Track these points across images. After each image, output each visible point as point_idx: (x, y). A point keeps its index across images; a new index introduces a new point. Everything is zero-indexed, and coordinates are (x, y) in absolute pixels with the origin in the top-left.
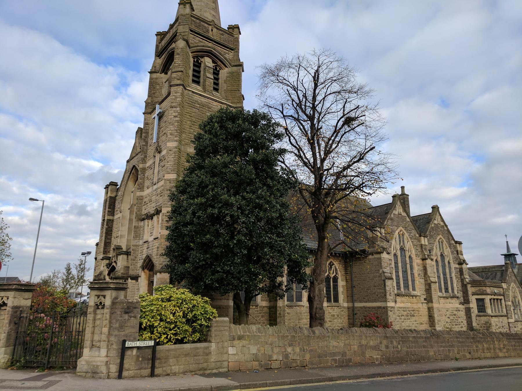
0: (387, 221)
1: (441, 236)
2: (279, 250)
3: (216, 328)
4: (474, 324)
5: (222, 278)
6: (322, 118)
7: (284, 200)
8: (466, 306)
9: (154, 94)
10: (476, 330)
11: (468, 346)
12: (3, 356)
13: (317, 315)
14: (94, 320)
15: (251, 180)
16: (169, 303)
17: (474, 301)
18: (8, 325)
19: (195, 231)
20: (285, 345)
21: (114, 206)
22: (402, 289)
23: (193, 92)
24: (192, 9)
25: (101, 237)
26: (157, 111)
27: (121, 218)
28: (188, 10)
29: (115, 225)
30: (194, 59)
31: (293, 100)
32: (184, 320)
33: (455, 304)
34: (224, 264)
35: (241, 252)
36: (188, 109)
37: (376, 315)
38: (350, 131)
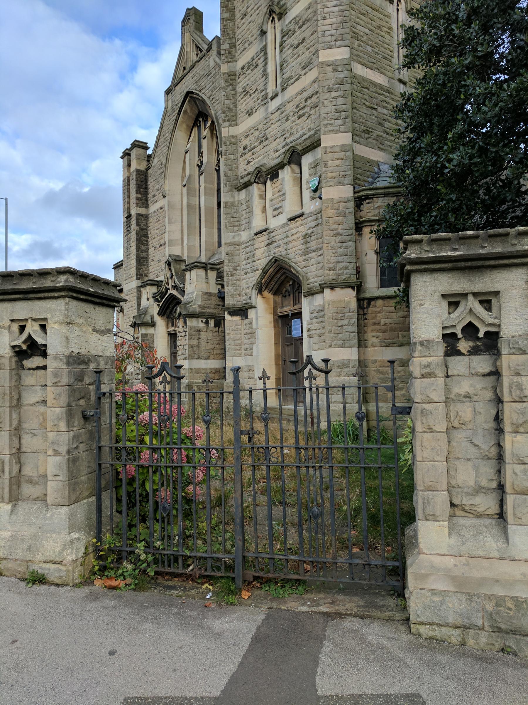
12: (65, 536)
18: (63, 426)
21: (146, 188)
25: (127, 248)
27: (166, 208)
29: (152, 224)
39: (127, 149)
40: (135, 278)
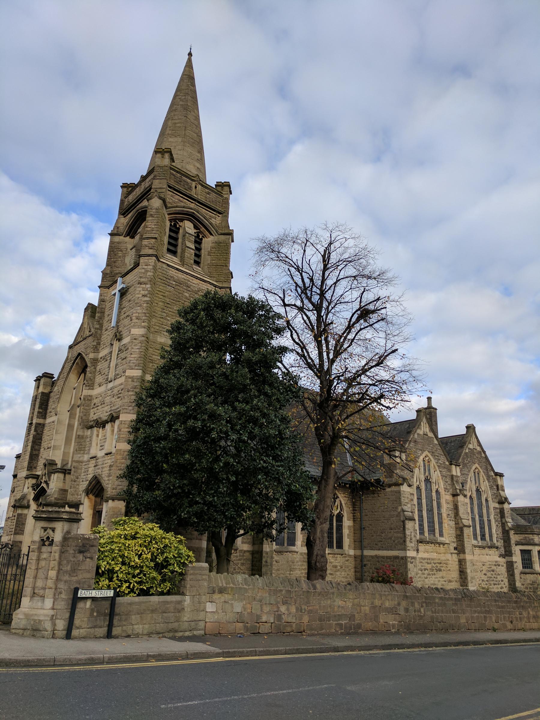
0: (409, 444)
1: (477, 465)
2: (275, 478)
3: (192, 577)
4: (518, 584)
5: (202, 511)
6: (332, 308)
7: (283, 412)
8: (508, 559)
9: (115, 262)
10: (520, 592)
11: (509, 613)
13: (318, 564)
14: (38, 560)
15: (245, 386)
16: (134, 541)
17: (518, 553)
19: (170, 449)
20: (277, 603)
21: (47, 405)
22: (426, 534)
23: (168, 265)
24: (172, 160)
25: (25, 446)
26: (119, 286)
27: (56, 423)
28: (166, 161)
30: (171, 222)
31: (297, 285)
32: (152, 564)
33: (493, 556)
34: (206, 494)
35: (228, 477)
36: (161, 287)
37: (392, 567)
38: (367, 327)
39: (39, 376)
40: (26, 469)
